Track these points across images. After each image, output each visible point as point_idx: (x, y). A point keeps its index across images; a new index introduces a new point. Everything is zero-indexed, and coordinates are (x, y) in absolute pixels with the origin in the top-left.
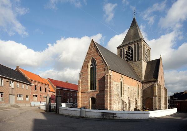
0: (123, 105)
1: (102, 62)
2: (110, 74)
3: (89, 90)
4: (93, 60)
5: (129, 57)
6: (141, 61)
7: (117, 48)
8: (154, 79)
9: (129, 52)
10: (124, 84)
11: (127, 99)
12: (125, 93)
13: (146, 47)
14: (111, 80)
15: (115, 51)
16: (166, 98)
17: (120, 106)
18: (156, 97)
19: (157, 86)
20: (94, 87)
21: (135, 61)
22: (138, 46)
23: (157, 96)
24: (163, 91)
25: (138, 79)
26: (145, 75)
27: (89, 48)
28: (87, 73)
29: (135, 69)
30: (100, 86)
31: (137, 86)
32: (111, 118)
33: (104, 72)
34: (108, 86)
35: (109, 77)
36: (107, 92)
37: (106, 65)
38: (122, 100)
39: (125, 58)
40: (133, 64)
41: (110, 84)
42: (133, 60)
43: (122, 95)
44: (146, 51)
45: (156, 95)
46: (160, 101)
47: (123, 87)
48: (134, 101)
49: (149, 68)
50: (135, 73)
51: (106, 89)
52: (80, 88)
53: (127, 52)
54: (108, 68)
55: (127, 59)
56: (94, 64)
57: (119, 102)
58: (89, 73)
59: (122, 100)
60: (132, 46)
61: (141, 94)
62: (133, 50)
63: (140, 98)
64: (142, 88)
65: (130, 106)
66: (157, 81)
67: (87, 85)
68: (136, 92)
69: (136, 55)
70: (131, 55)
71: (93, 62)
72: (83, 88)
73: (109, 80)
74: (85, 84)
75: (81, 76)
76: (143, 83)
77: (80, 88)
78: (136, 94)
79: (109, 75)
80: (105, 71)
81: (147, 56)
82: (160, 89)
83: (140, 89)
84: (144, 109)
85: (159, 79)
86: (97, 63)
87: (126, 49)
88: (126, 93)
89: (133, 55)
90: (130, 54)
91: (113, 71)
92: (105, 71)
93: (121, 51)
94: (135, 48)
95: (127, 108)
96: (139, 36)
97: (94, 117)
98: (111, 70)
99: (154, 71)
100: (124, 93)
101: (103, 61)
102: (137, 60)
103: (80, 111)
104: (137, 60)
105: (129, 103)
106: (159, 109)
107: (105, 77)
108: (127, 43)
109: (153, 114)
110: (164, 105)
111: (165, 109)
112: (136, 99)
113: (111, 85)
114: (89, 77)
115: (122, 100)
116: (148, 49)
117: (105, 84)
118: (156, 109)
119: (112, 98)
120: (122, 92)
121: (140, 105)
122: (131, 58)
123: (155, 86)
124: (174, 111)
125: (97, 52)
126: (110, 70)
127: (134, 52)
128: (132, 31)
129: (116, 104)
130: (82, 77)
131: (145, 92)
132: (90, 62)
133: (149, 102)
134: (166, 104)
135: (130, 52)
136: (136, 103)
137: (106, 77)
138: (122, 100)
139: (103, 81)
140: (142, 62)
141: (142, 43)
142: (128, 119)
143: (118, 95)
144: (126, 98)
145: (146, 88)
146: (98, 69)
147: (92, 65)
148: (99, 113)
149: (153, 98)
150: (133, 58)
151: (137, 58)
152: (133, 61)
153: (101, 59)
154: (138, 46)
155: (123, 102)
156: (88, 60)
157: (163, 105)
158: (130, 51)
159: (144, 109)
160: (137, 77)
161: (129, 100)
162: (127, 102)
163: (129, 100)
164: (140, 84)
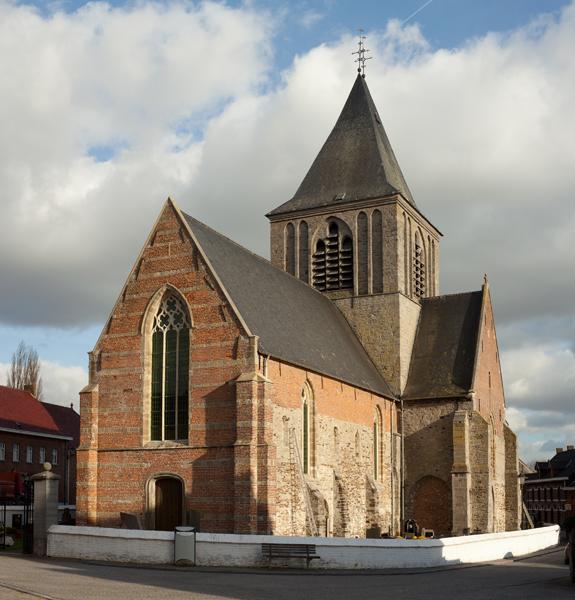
0: (316, 514)
1: (222, 314)
2: (261, 375)
3: (147, 440)
4: (172, 299)
5: (331, 269)
6: (388, 299)
7: (267, 216)
8: (453, 391)
9: (331, 247)
10: (318, 417)
11: (330, 482)
12: (320, 459)
13: (415, 229)
14: (268, 402)
15: (259, 241)
16: (510, 477)
17: (301, 517)
18: (464, 473)
19: (467, 423)
20: (173, 418)
21: (364, 293)
22: (378, 227)
23: (469, 469)
24: (498, 445)
25: (380, 387)
26: (415, 350)
27: (152, 241)
28: (136, 359)
29: (360, 331)
30: (205, 420)
31: (376, 418)
32: (294, 562)
33: (230, 362)
34: (250, 429)
35: (255, 386)
36: (248, 454)
37: (243, 332)
38: (312, 492)
39: (312, 260)
40: (356, 309)
41: (261, 419)
42: (352, 287)
43: (310, 468)
44: (417, 247)
45: (465, 467)
46: (481, 491)
47: (314, 430)
48: (363, 492)
49: (433, 332)
50: (363, 355)
51: (239, 442)
52: (95, 426)
53: (321, 245)
54: (251, 348)
55: (324, 278)
56: (178, 319)
57: (295, 500)
58: (148, 359)
59: (309, 488)
60: (351, 219)
61: (393, 460)
62: (356, 239)
63: (386, 476)
64: (399, 430)
65: (343, 515)
66: (470, 399)
67: (139, 415)
68: (371, 449)
69: (371, 266)
70: (344, 275)
71: (171, 306)
72: (110, 431)
73: (255, 402)
74: (123, 408)
75: (99, 369)
76: (403, 403)
77: (95, 426)
78: (372, 456)
79: (255, 378)
80: (234, 357)
81: (420, 271)
82: (482, 436)
83: (387, 441)
84: (408, 529)
85: (479, 390)
86: (195, 317)
87: (320, 230)
88: (323, 455)
89: (351, 260)
90: (336, 254)
91: (271, 358)
92: (234, 357)
93: (291, 237)
94: (364, 230)
95: (331, 528)
96: (383, 175)
97: (227, 563)
98: (265, 356)
99: (454, 352)
100: (317, 456)
101: (225, 311)
102: (371, 291)
103: (174, 542)
104: (371, 291)
105: (341, 505)
106: (477, 532)
107: (235, 387)
108: (325, 198)
109: (458, 550)
110: (504, 512)
111: (508, 529)
112: (368, 483)
113: (267, 424)
114: (148, 376)
115: (309, 488)
116: (425, 234)
117: (234, 418)
118: (465, 532)
119: (270, 483)
120: (306, 449)
121: (388, 510)
122: (344, 275)
123: (461, 424)
124: (548, 536)
125: (197, 268)
126: (259, 354)
127: (356, 248)
128: (350, 144)
129: (284, 509)
130: (103, 373)
131: (412, 448)
132: (156, 307)
133: (431, 501)
134: (510, 506)
135: (336, 247)
136: (372, 504)
137: (239, 388)
138: (312, 492)
139: (228, 401)
140: (396, 305)
141: (400, 210)
142: (359, 567)
143: (292, 468)
144: (323, 479)
145: (416, 427)
146: (196, 346)
147: (165, 320)
148: (248, 547)
149: (450, 478)
150: (351, 275)
151: (371, 279)
152: (353, 293)
153: (218, 302)
154: (378, 227)
155: (316, 498)
156: (147, 295)
157: (498, 513)
158: (336, 239)
159: (408, 529)
160: (370, 376)
161: (340, 489)
162: (329, 495)
163: (340, 489)
164: (389, 410)
